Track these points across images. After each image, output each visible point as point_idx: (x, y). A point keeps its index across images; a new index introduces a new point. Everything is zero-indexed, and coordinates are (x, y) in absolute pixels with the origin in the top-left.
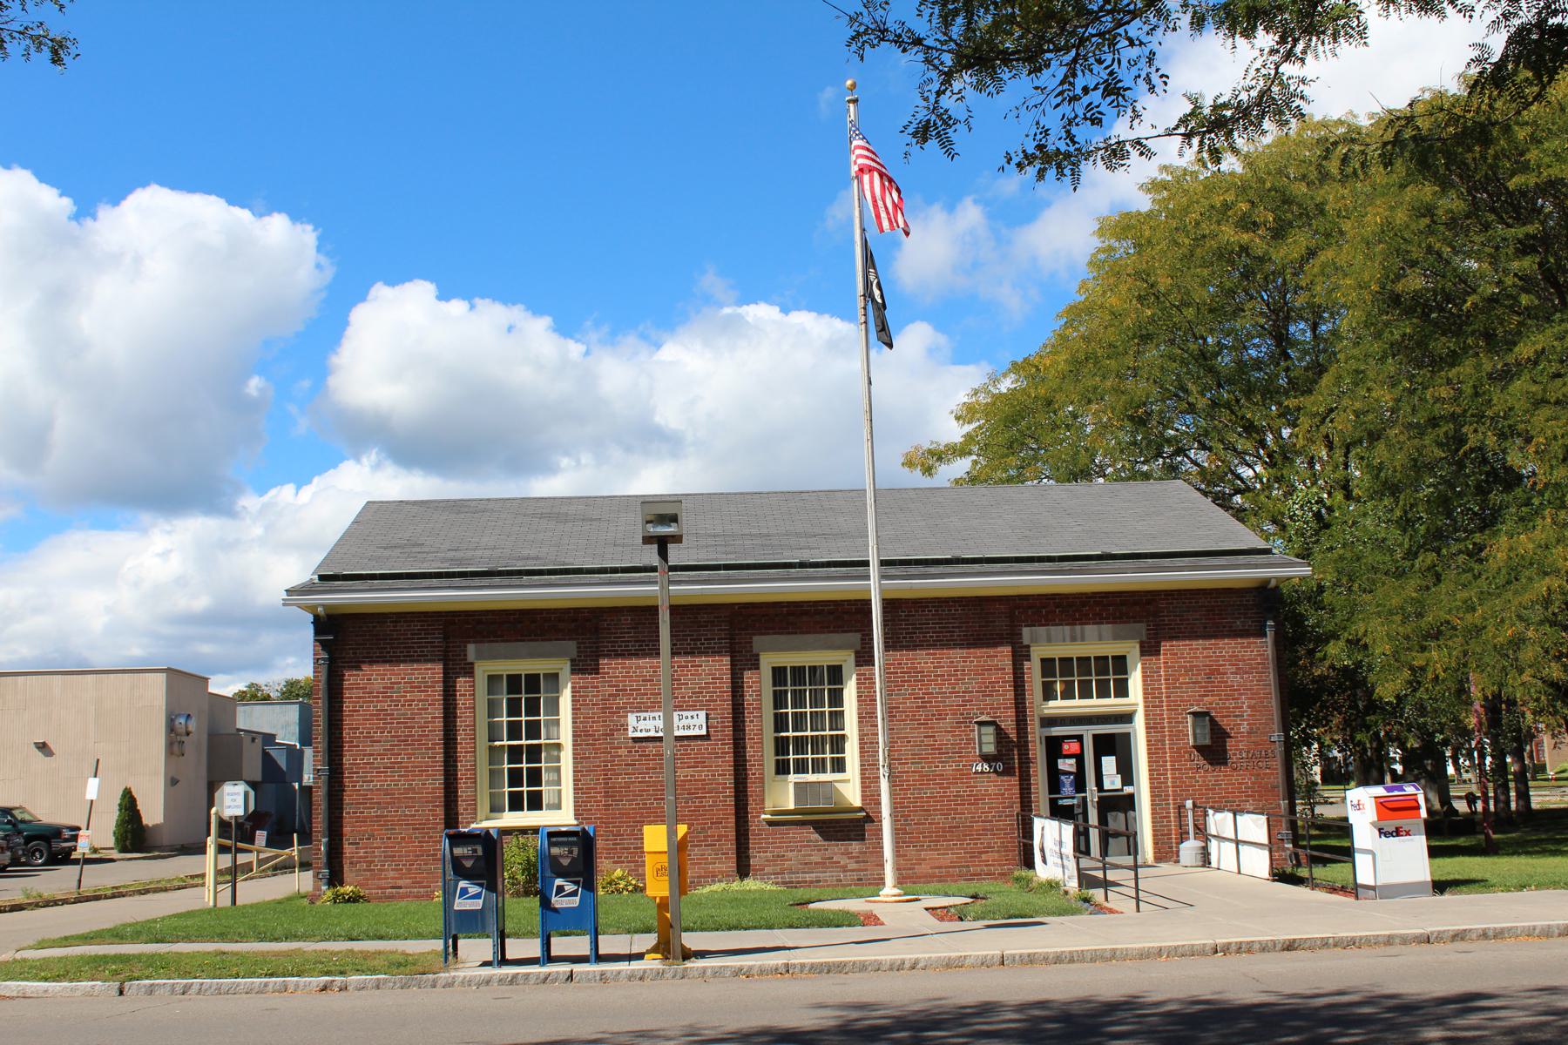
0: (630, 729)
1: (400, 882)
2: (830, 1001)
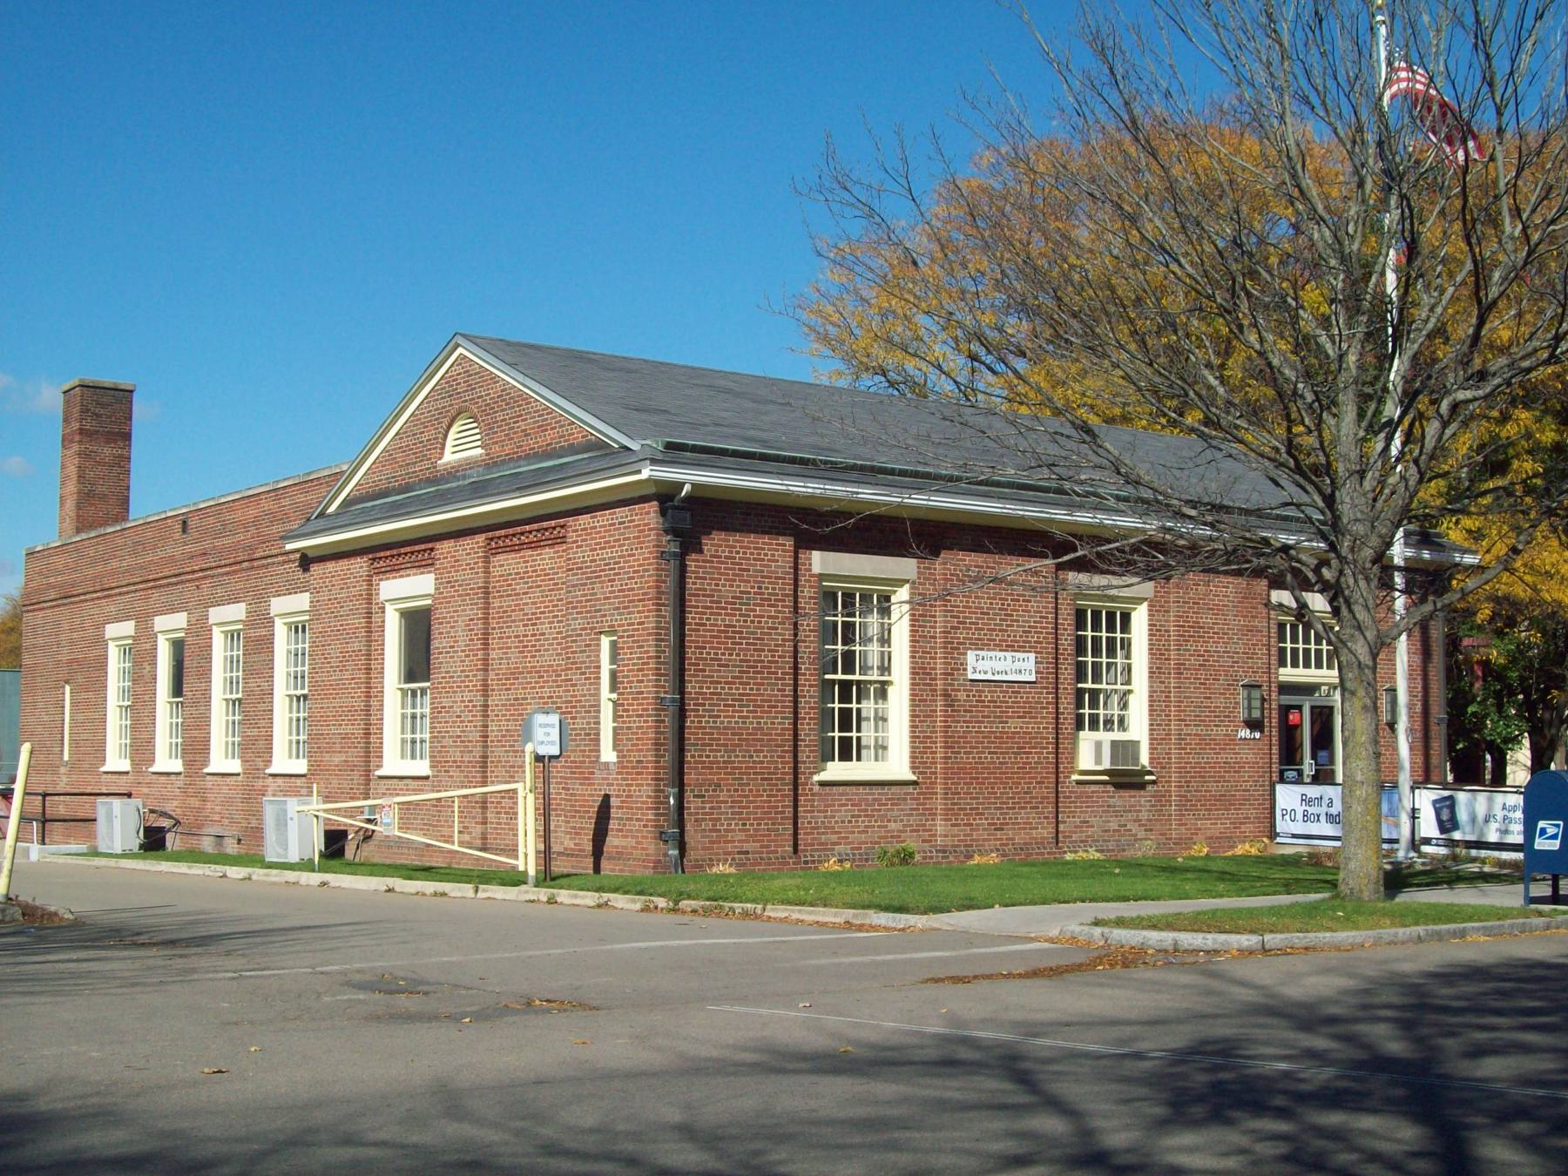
0: (970, 669)
1: (746, 847)
2: (1133, 1015)
